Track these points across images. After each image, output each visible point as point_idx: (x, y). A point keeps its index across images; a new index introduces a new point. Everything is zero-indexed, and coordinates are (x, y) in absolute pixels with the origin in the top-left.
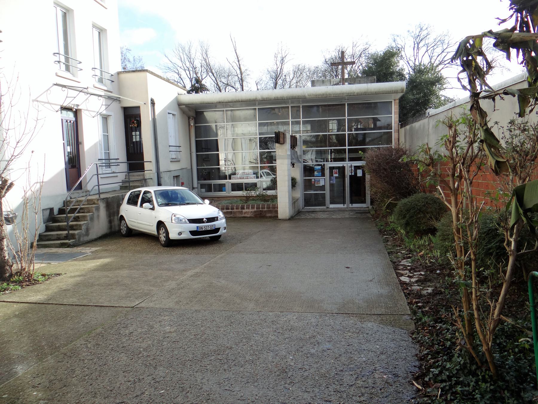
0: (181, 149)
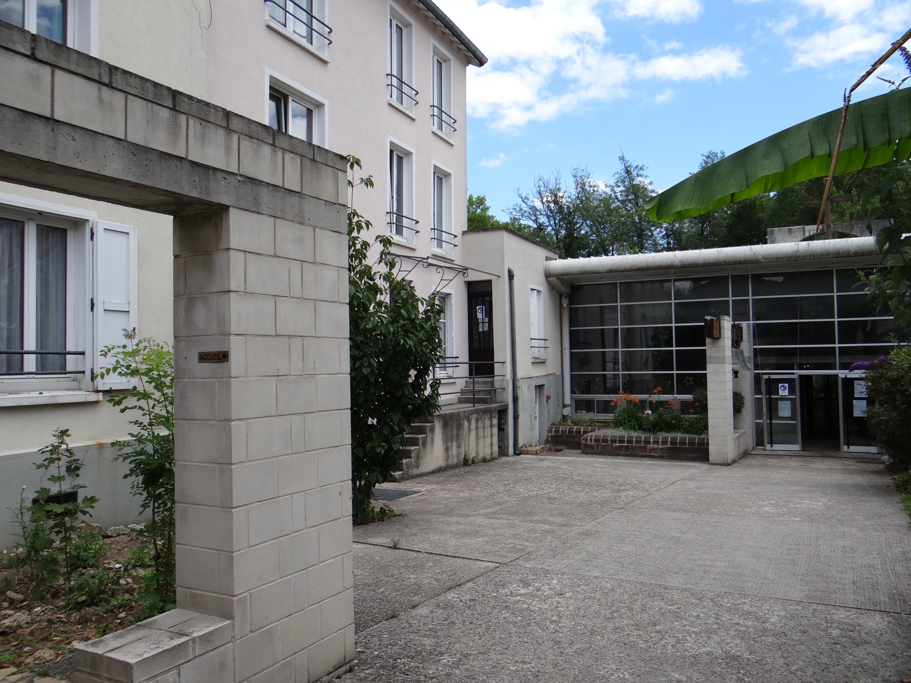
0: (548, 344)
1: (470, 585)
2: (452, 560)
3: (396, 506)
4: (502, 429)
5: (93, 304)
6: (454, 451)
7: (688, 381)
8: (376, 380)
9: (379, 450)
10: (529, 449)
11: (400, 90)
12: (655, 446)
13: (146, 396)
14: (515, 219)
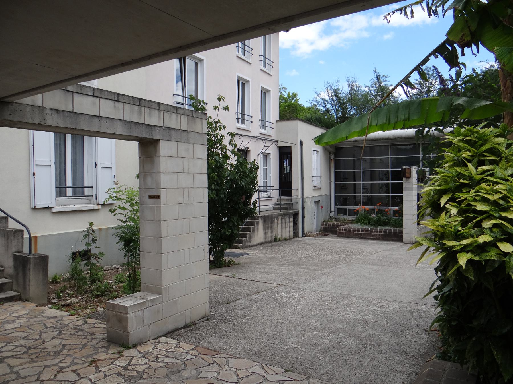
0: (322, 179)
1: (264, 292)
2: (258, 283)
3: (236, 260)
4: (295, 223)
5: (96, 165)
6: (269, 234)
7: (397, 199)
8: (227, 200)
9: (227, 233)
10: (310, 234)
11: (244, 49)
12: (376, 233)
13: (124, 209)
14: (315, 105)
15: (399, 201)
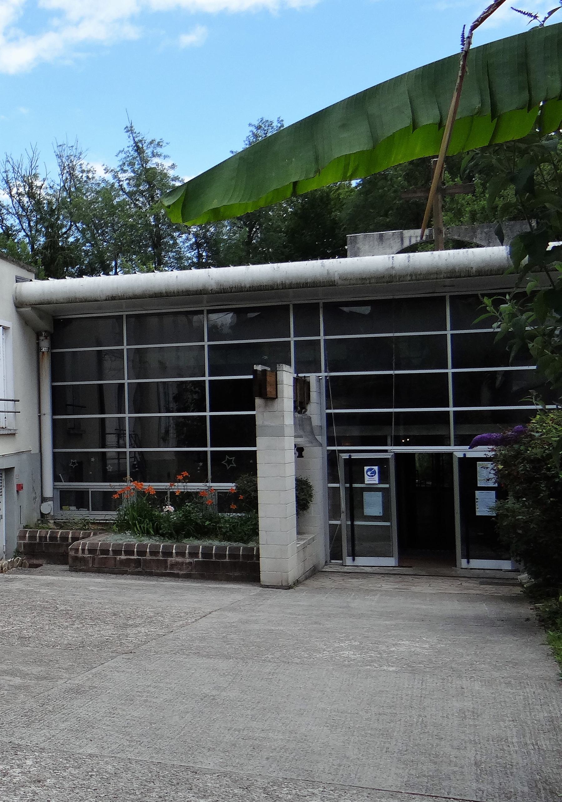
0: (19, 406)
7: (229, 462)
12: (180, 559)
15: (245, 467)
